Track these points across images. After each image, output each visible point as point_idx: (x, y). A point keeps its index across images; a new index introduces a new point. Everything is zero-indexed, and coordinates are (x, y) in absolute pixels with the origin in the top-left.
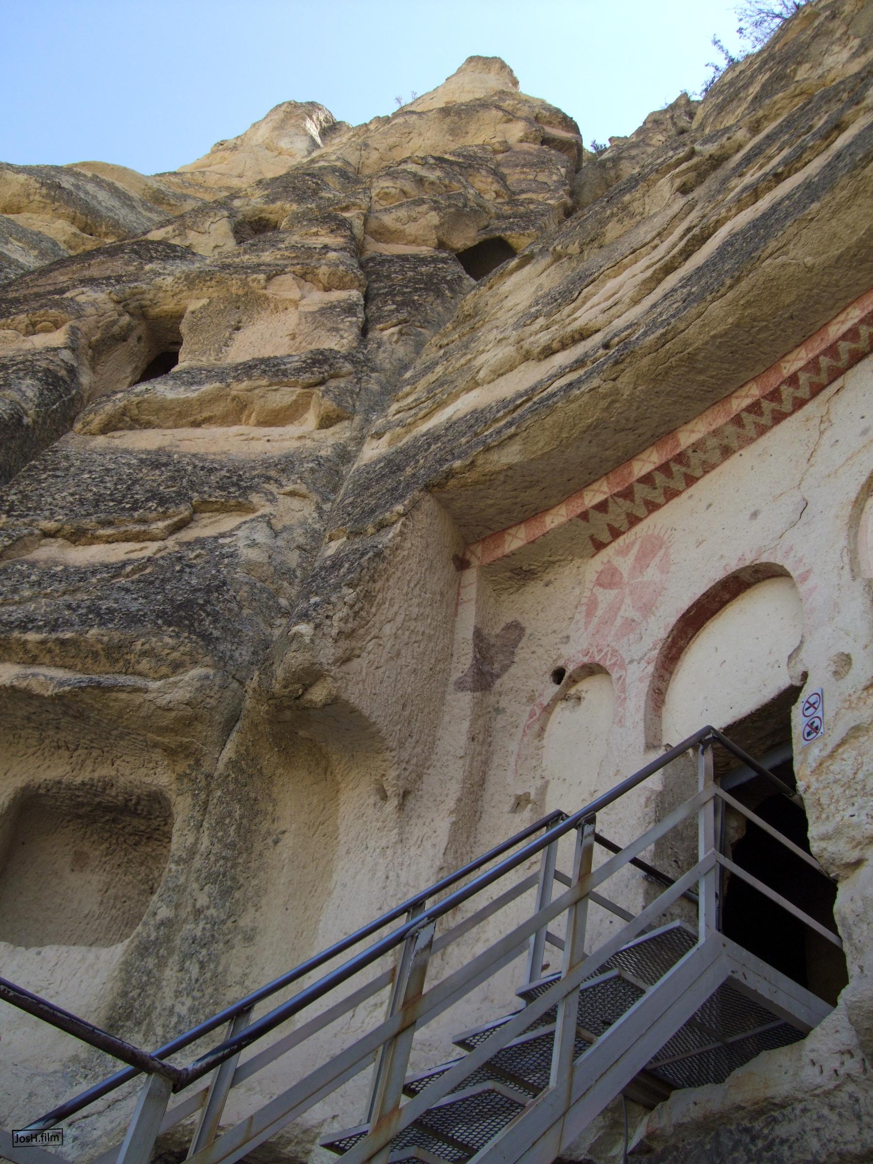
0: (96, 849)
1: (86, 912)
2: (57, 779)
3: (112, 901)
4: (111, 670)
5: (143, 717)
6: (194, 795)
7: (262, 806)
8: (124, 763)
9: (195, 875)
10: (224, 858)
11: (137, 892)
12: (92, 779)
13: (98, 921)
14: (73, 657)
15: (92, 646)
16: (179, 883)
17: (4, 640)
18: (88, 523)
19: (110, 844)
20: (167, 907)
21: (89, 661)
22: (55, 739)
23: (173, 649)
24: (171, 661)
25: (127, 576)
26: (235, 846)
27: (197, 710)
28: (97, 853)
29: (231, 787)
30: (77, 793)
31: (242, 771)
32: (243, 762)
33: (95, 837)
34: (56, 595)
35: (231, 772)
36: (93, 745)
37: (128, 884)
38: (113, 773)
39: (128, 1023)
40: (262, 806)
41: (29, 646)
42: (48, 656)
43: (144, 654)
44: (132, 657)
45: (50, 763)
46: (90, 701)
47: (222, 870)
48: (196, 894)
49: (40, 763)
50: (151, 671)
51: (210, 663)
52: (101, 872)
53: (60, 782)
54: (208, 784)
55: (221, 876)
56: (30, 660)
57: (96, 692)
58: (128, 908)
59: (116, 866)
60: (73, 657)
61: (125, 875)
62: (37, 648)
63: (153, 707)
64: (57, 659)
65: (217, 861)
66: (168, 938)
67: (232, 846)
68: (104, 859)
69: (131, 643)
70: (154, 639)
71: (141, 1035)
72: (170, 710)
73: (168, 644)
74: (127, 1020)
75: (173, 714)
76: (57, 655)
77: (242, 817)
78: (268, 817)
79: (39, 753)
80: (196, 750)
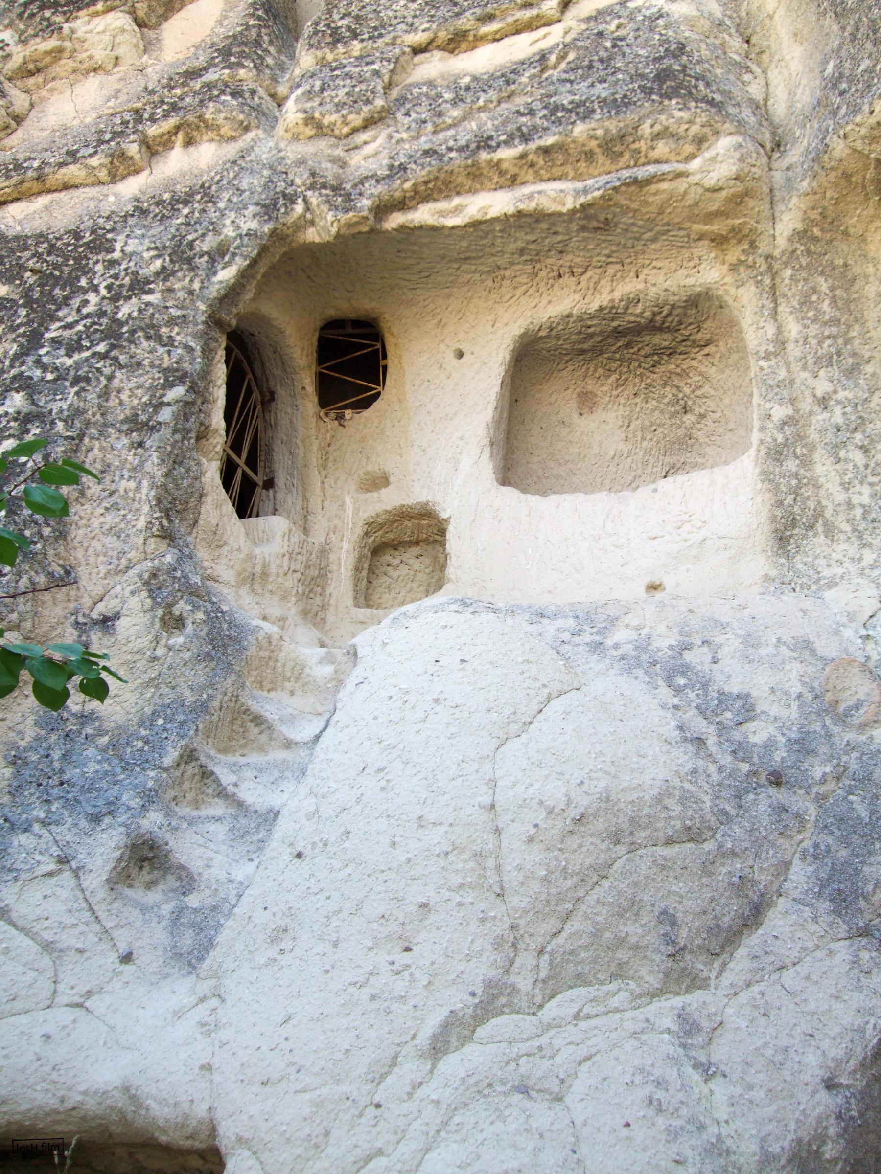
0: (603, 385)
1: (612, 453)
2: (565, 313)
3: (639, 434)
4: (613, 167)
5: (690, 206)
6: (757, 282)
7: (857, 270)
8: (655, 271)
9: (800, 364)
10: (829, 337)
11: (667, 416)
12: (612, 301)
13: (629, 459)
14: (562, 165)
15: (584, 145)
16: (781, 378)
17: (473, 165)
18: (466, 22)
19: (620, 374)
20: (781, 405)
21: (583, 165)
22: (555, 268)
23: (691, 122)
24: (694, 137)
25: (555, 68)
26: (839, 321)
27: (746, 183)
28: (605, 389)
29: (804, 261)
30: (589, 323)
31: (816, 240)
32: (815, 230)
33: (600, 371)
34: (491, 106)
35: (798, 245)
36: (611, 260)
37: (653, 411)
38: (641, 286)
39: (796, 531)
40: (857, 270)
41: (504, 166)
42: (530, 171)
43: (657, 136)
44: (642, 145)
45: (550, 298)
46: (625, 202)
47: (833, 350)
48: (811, 382)
49: (536, 301)
50: (673, 154)
51: (733, 130)
52: (615, 407)
53: (569, 316)
54: (770, 267)
55: (835, 357)
56: (509, 183)
57: (633, 188)
58: (661, 436)
59: (632, 396)
60: (562, 165)
61: (647, 402)
62: (516, 165)
63: (700, 191)
64: (543, 172)
65: (820, 343)
66: (799, 436)
67: (835, 322)
68: (615, 393)
69: (636, 128)
70: (663, 117)
71: (822, 537)
72: (720, 189)
73: (682, 118)
74: (794, 527)
75: (724, 194)
76: (541, 168)
77: (832, 289)
78: (871, 279)
79: (531, 291)
80: (751, 230)
